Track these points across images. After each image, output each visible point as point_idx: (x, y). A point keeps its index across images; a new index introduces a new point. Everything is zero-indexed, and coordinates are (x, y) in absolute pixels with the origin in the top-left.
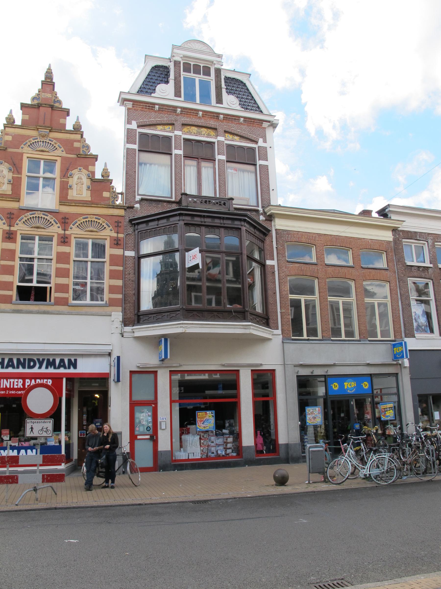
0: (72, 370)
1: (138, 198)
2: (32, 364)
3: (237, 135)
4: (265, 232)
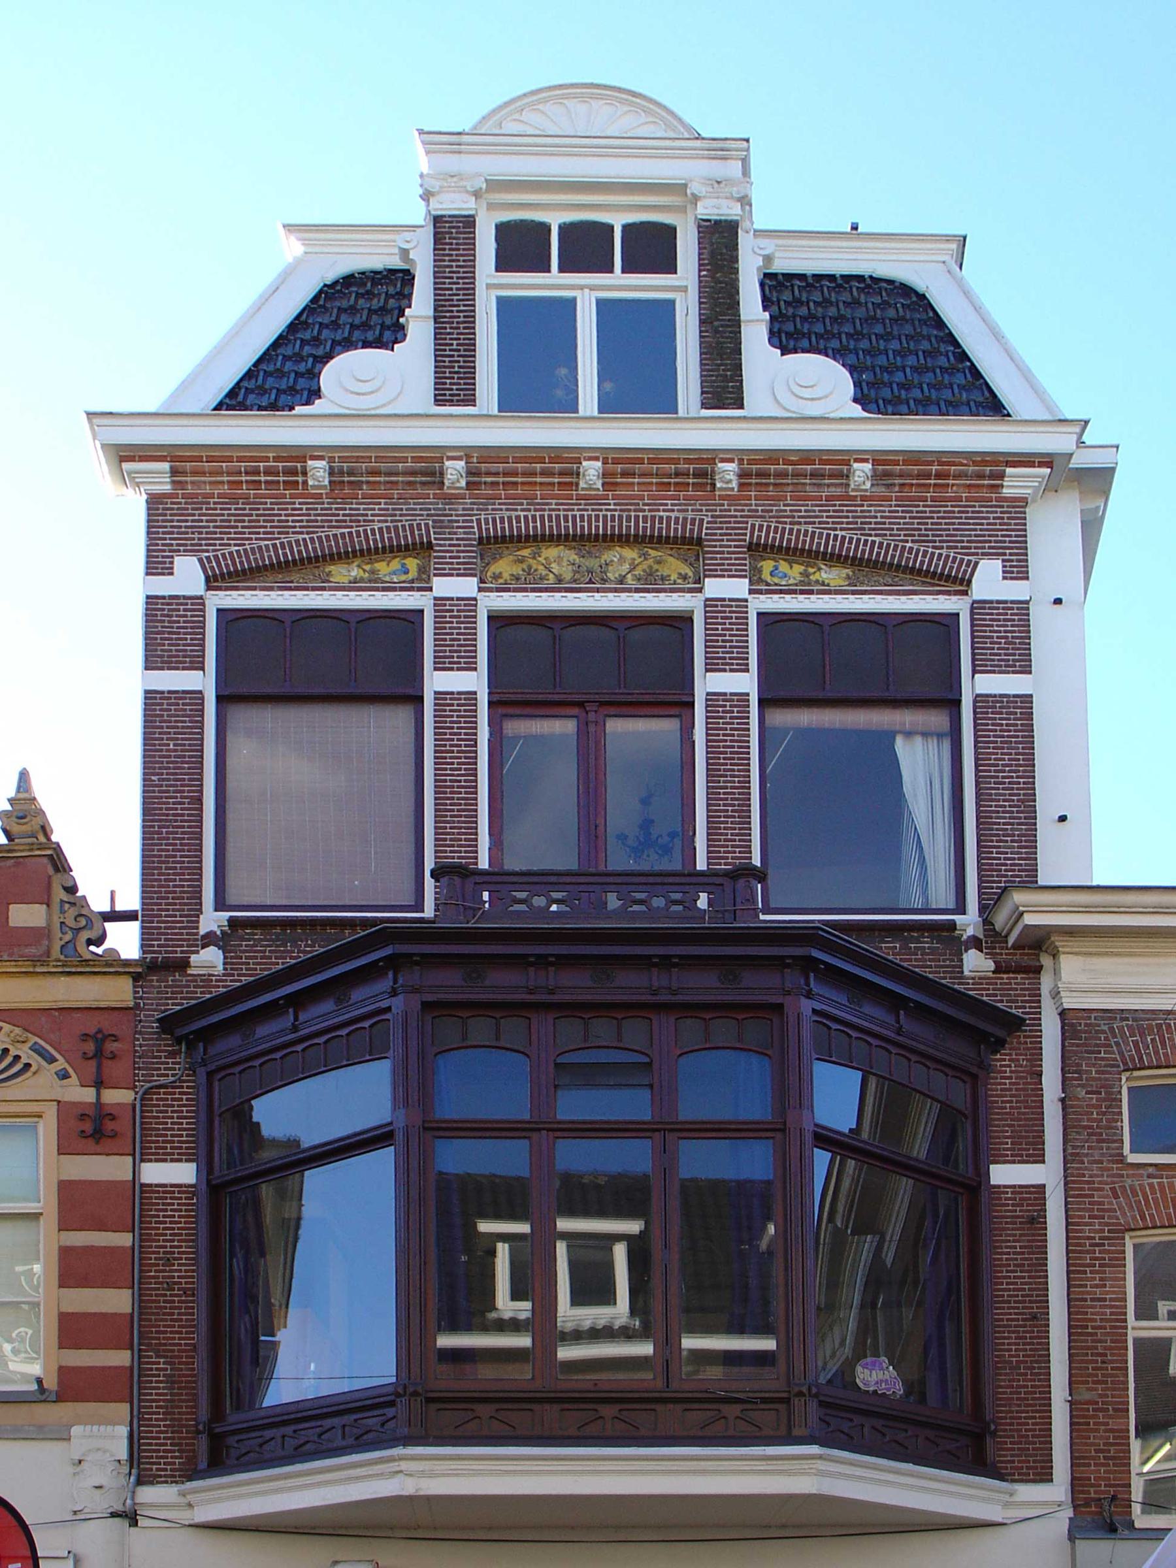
1: (212, 920)
3: (835, 559)
4: (990, 1028)
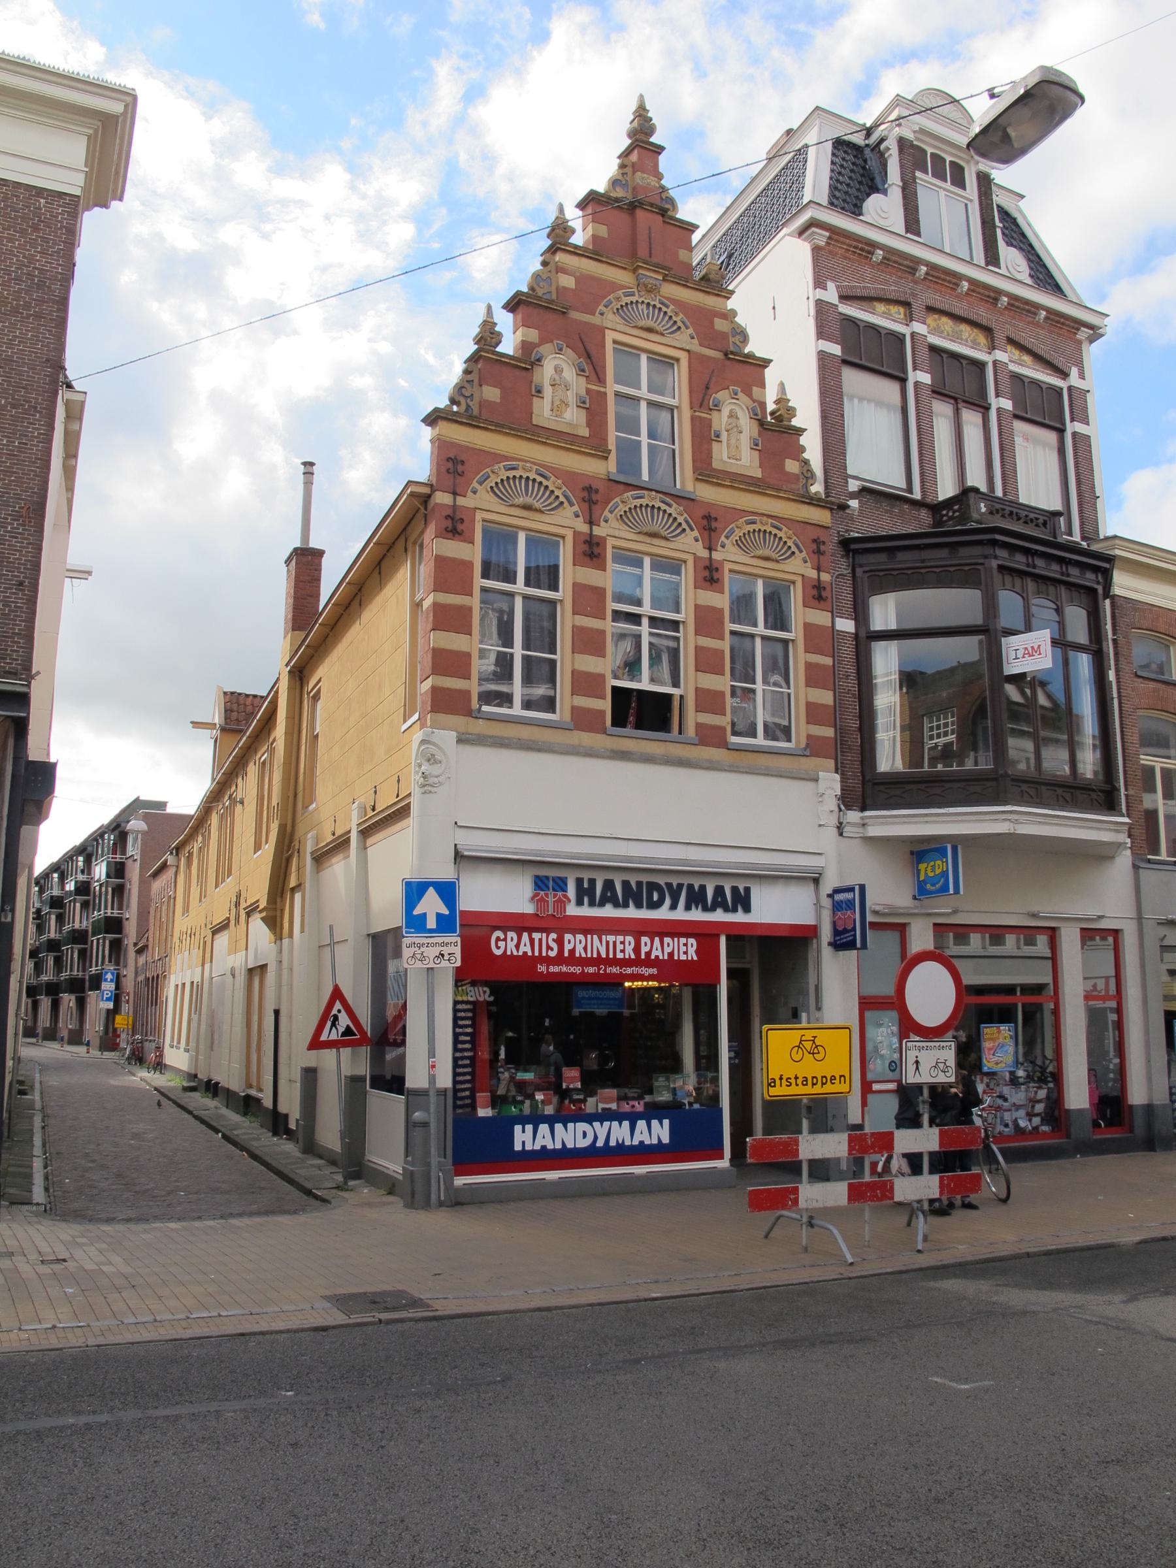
0: (739, 917)
1: (853, 486)
2: (656, 897)
